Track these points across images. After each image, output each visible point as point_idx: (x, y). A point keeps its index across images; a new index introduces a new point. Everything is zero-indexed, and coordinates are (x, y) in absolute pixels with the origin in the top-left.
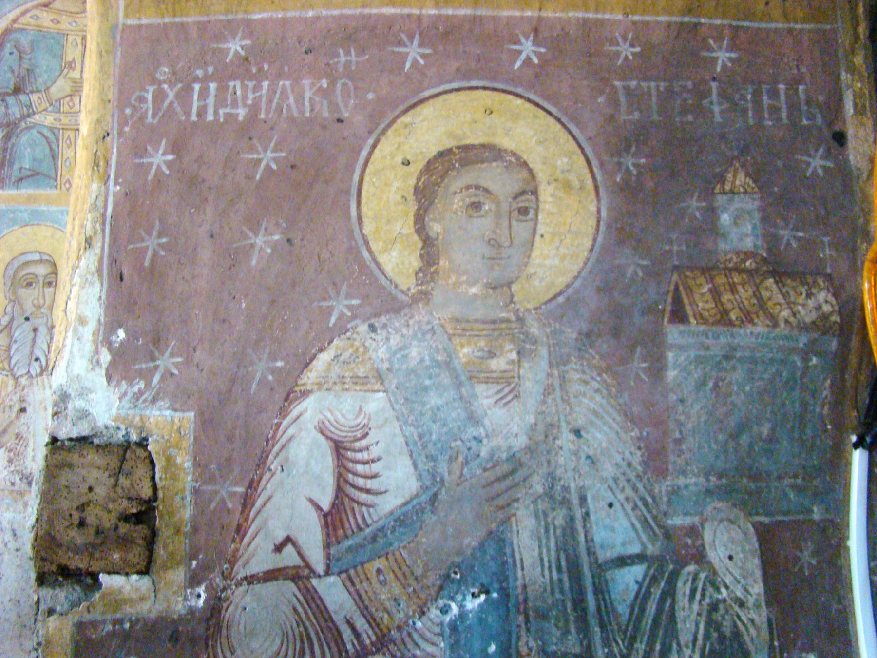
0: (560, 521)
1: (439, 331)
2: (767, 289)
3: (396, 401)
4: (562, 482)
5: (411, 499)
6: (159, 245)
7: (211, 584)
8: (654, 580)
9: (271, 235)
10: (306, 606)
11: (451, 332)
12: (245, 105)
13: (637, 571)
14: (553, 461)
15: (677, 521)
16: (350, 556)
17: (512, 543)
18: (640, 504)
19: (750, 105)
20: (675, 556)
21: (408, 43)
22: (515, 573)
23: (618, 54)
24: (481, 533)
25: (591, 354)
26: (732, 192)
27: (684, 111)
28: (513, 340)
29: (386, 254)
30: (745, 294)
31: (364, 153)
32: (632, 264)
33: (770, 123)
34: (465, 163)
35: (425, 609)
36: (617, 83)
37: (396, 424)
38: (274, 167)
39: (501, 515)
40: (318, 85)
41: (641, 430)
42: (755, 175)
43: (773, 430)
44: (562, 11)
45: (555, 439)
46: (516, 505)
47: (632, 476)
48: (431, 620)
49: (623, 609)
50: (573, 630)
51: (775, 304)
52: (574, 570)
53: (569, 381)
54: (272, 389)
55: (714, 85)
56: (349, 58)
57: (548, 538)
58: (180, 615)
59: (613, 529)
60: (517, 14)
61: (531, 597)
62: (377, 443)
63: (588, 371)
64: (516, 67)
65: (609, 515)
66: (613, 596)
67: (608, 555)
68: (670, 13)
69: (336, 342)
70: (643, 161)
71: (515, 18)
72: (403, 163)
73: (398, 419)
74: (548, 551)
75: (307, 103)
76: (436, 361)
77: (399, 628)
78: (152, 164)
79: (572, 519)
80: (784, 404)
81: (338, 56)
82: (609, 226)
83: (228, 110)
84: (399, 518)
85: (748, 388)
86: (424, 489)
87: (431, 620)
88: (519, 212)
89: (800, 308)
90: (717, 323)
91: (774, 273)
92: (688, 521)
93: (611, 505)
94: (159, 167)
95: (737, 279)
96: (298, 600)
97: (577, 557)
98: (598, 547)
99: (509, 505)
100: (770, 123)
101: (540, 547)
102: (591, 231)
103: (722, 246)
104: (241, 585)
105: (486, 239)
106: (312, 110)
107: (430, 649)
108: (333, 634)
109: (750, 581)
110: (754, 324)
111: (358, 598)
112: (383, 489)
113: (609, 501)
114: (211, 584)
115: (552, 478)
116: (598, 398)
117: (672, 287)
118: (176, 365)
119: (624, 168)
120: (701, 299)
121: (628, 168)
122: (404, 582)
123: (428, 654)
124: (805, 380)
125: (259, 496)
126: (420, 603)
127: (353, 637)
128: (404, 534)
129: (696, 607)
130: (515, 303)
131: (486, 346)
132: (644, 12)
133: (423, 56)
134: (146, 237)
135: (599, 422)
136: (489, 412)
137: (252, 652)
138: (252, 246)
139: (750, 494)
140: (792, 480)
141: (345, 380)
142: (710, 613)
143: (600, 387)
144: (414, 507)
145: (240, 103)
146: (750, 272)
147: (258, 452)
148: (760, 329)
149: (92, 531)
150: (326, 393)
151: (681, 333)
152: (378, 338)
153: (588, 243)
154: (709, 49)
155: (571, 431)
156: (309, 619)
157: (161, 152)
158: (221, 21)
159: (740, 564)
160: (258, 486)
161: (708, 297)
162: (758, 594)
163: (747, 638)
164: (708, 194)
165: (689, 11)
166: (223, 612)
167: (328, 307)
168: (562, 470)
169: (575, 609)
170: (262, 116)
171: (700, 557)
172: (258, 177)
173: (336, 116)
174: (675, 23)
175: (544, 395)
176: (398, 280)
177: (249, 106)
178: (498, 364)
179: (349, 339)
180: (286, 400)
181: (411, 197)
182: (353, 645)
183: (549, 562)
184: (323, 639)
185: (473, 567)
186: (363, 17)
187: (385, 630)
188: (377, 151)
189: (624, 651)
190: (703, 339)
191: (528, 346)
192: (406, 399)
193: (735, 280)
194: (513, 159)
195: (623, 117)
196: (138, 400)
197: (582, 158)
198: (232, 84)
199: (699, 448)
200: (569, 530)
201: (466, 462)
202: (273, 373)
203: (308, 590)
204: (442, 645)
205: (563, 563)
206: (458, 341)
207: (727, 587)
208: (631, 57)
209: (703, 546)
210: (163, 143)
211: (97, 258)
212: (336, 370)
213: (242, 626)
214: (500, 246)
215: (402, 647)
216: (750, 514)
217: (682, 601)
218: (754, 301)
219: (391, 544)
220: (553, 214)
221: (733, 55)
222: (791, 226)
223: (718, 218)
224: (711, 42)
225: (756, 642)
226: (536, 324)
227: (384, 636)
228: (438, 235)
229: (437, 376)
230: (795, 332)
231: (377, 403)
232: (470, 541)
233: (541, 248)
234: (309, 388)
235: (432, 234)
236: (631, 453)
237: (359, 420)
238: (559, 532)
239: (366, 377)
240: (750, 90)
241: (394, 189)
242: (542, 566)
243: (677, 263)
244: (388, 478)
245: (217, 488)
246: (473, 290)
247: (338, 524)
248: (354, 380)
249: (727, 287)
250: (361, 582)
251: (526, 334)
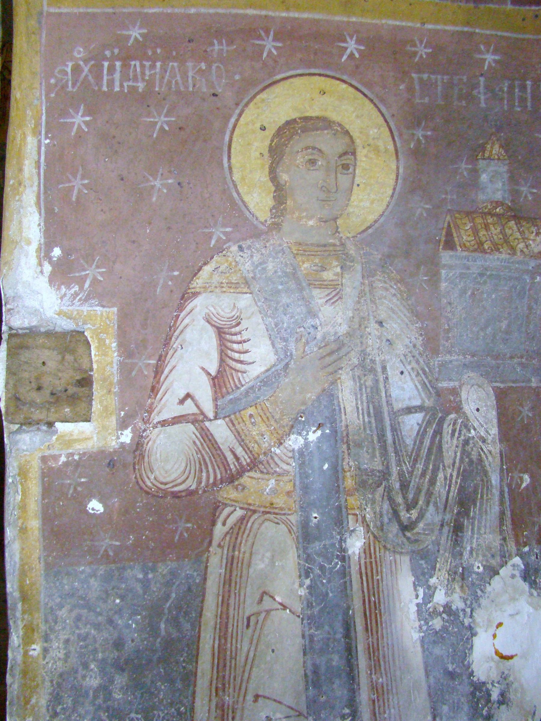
0: (369, 383)
1: (287, 251)
2: (510, 228)
3: (259, 300)
4: (370, 357)
5: (271, 367)
6: (83, 185)
7: (135, 427)
8: (429, 423)
9: (167, 179)
10: (202, 440)
11: (295, 252)
12: (143, 80)
13: (418, 417)
14: (364, 342)
15: (444, 384)
16: (231, 406)
17: (338, 397)
18: (420, 372)
19: (505, 95)
20: (443, 406)
22: (341, 417)
23: (415, 53)
24: (318, 389)
25: (390, 270)
26: (489, 158)
27: (460, 98)
28: (337, 259)
29: (250, 195)
30: (495, 231)
31: (233, 120)
32: (420, 207)
33: (519, 109)
34: (305, 130)
35: (282, 441)
36: (414, 75)
37: (260, 316)
38: (167, 128)
39: (330, 378)
40: (198, 67)
41: (422, 323)
42: (505, 146)
43: (509, 326)
45: (366, 327)
46: (340, 372)
47: (416, 353)
48: (286, 448)
49: (409, 441)
50: (378, 455)
51: (514, 239)
52: (378, 415)
53: (375, 288)
54: (172, 291)
55: (482, 79)
56: (221, 47)
57: (361, 394)
58: (114, 449)
59: (403, 389)
60: (345, 19)
61: (351, 433)
62: (247, 329)
63: (388, 281)
64: (343, 60)
65: (401, 380)
66: (403, 434)
67: (400, 406)
68: (454, 24)
69: (215, 258)
70: (429, 133)
71: (344, 22)
72: (261, 129)
73: (260, 312)
74: (362, 403)
75: (190, 80)
76: (286, 273)
77: (265, 453)
78: (74, 123)
79: (377, 381)
80: (517, 308)
81: (213, 45)
82: (405, 179)
83: (130, 83)
84: (263, 380)
85: (494, 296)
86: (279, 360)
87: (286, 448)
88: (342, 167)
89: (531, 242)
90: (475, 251)
91: (515, 217)
92: (452, 384)
93: (402, 373)
94: (79, 125)
95: (490, 220)
96: (197, 437)
97: (380, 406)
98: (393, 400)
99: (336, 371)
100: (519, 109)
101: (356, 399)
102: (392, 182)
103: (481, 197)
104: (157, 427)
105: (319, 186)
106: (194, 86)
107: (285, 467)
108: (221, 459)
109: (489, 425)
110: (500, 253)
111: (238, 435)
112: (251, 361)
113: (401, 370)
114: (135, 427)
115: (364, 354)
116: (395, 300)
117: (446, 225)
118: (102, 274)
119: (416, 138)
120: (465, 235)
121: (418, 139)
122: (267, 423)
123: (285, 470)
124: (531, 292)
125: (166, 366)
126: (279, 437)
127: (234, 460)
128: (267, 391)
129: (455, 441)
130: (339, 233)
131: (319, 262)
132: (437, 22)
133: (276, 48)
134: (73, 180)
135: (394, 316)
136: (322, 308)
137: (166, 472)
138: (153, 187)
139: (492, 368)
140: (520, 360)
141: (223, 285)
142: (464, 446)
143: (396, 293)
144: (273, 373)
145: (140, 80)
146: (498, 216)
147: (164, 336)
148: (503, 256)
149: (48, 392)
150: (210, 294)
151: (451, 256)
152: (245, 255)
153: (390, 192)
154: (481, 52)
155: (376, 322)
156: (204, 449)
157: (80, 114)
159: (483, 415)
160: (165, 359)
161: (470, 232)
162: (494, 435)
163: (486, 463)
164: (473, 160)
165: (468, 24)
166: (145, 445)
167: (210, 233)
168: (371, 348)
169: (379, 442)
170: (157, 89)
171: (458, 408)
172: (155, 136)
173: (212, 91)
175: (358, 297)
176: (258, 214)
177: (147, 81)
178: (328, 275)
179: (224, 256)
180: (182, 299)
181: (266, 154)
182: (235, 465)
183: (362, 409)
184: (214, 463)
185: (313, 412)
187: (256, 455)
188: (242, 119)
189: (410, 469)
190: (465, 261)
191: (348, 263)
192: (266, 299)
193: (489, 221)
194: (339, 129)
195: (418, 101)
196: (74, 299)
197: (387, 130)
198: (133, 63)
199: (461, 336)
200: (375, 389)
201: (307, 343)
202: (171, 280)
203: (203, 429)
204: (294, 464)
205: (372, 411)
206: (300, 258)
207: (475, 429)
209: (461, 401)
210: (82, 107)
211: (35, 194)
212: (216, 278)
213: (158, 455)
214: (329, 192)
215: (267, 466)
216: (492, 382)
217: (446, 437)
218: (501, 236)
219: (258, 398)
220: (366, 170)
221: (497, 58)
222: (529, 184)
223: (479, 176)
225: (492, 465)
226: (353, 248)
227: (255, 459)
228: (286, 182)
229: (286, 283)
230: (527, 259)
231: (245, 301)
232: (311, 396)
233: (357, 195)
234: (198, 290)
235: (283, 182)
236: (416, 338)
237: (233, 313)
238: (369, 390)
239: (238, 283)
240: (506, 84)
241: (254, 148)
242: (358, 412)
243: (450, 208)
244: (255, 353)
245: (136, 361)
246: (311, 223)
247: (222, 384)
248: (229, 285)
249: (483, 226)
250: (239, 423)
251: (347, 254)
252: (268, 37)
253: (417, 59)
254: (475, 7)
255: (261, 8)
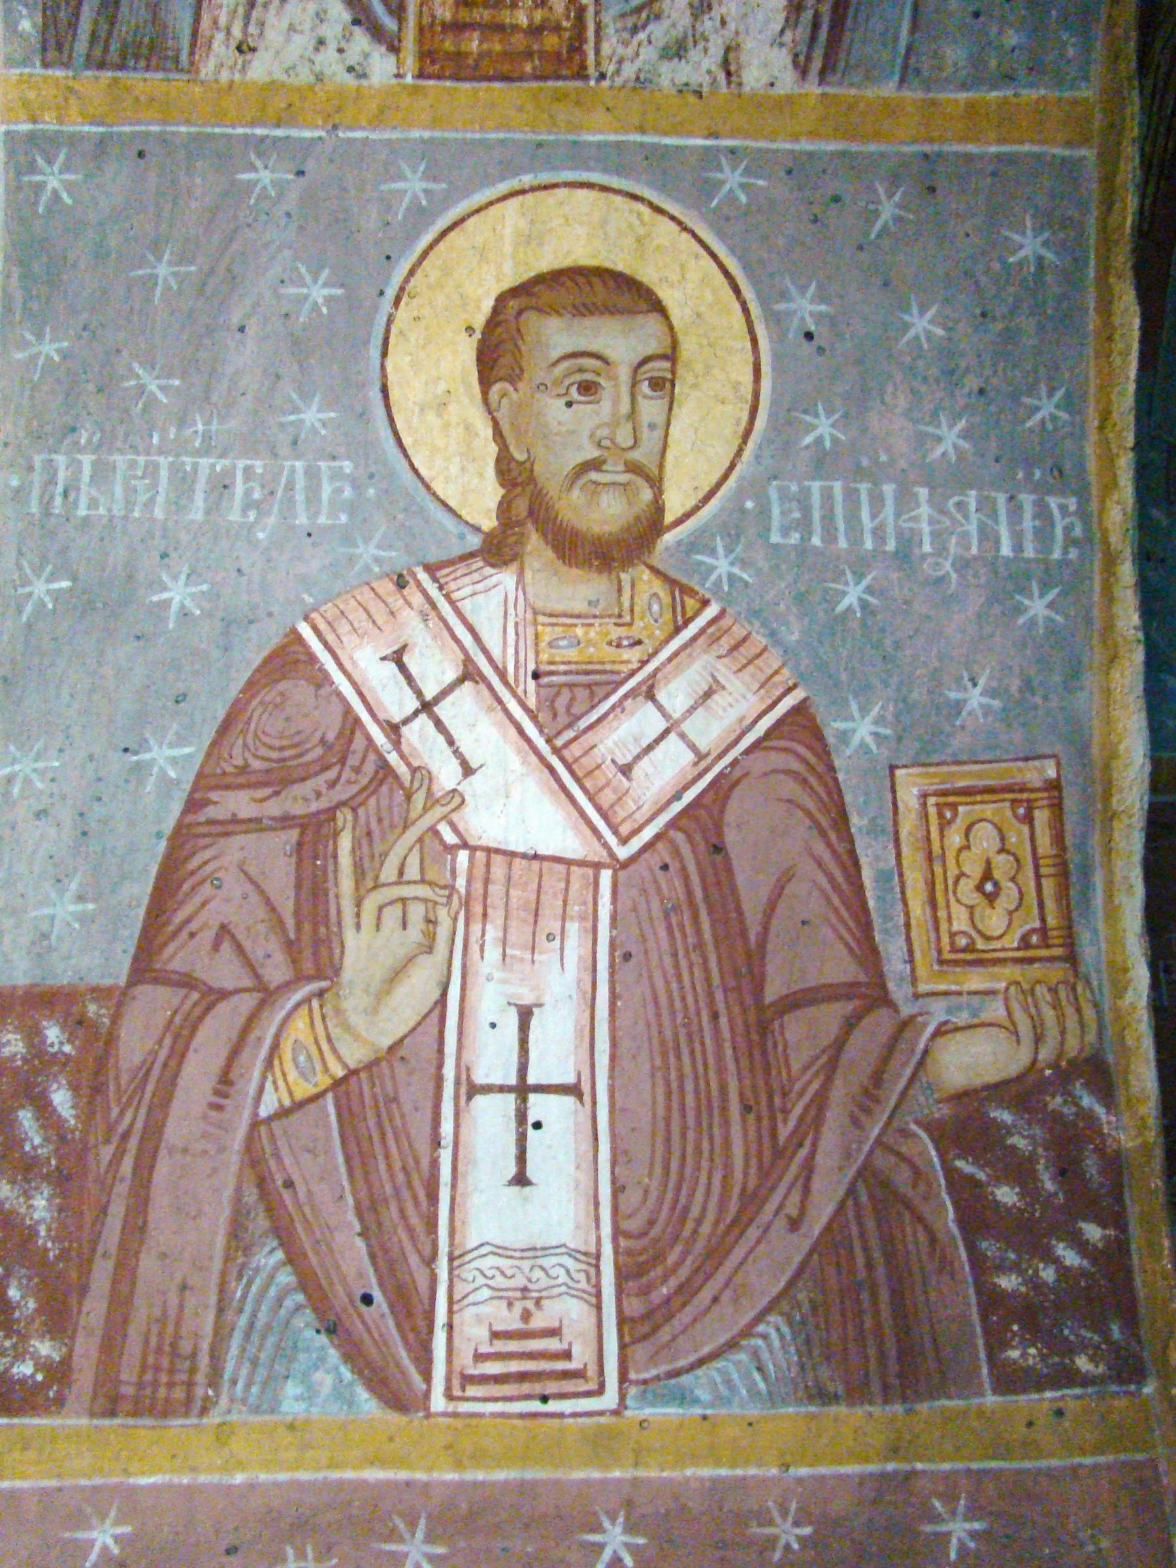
21: (407, 1536)
23: (773, 1541)
44: (673, 1467)
60: (596, 1475)
154: (937, 1518)
158: (83, 1489)
165: (894, 1451)
174: (871, 1475)
186: (327, 1484)
208: (796, 1546)
221: (977, 1526)
224: (937, 1504)
252: (413, 1534)
253: (777, 1556)
254: (909, 1411)
255: (402, 1462)
